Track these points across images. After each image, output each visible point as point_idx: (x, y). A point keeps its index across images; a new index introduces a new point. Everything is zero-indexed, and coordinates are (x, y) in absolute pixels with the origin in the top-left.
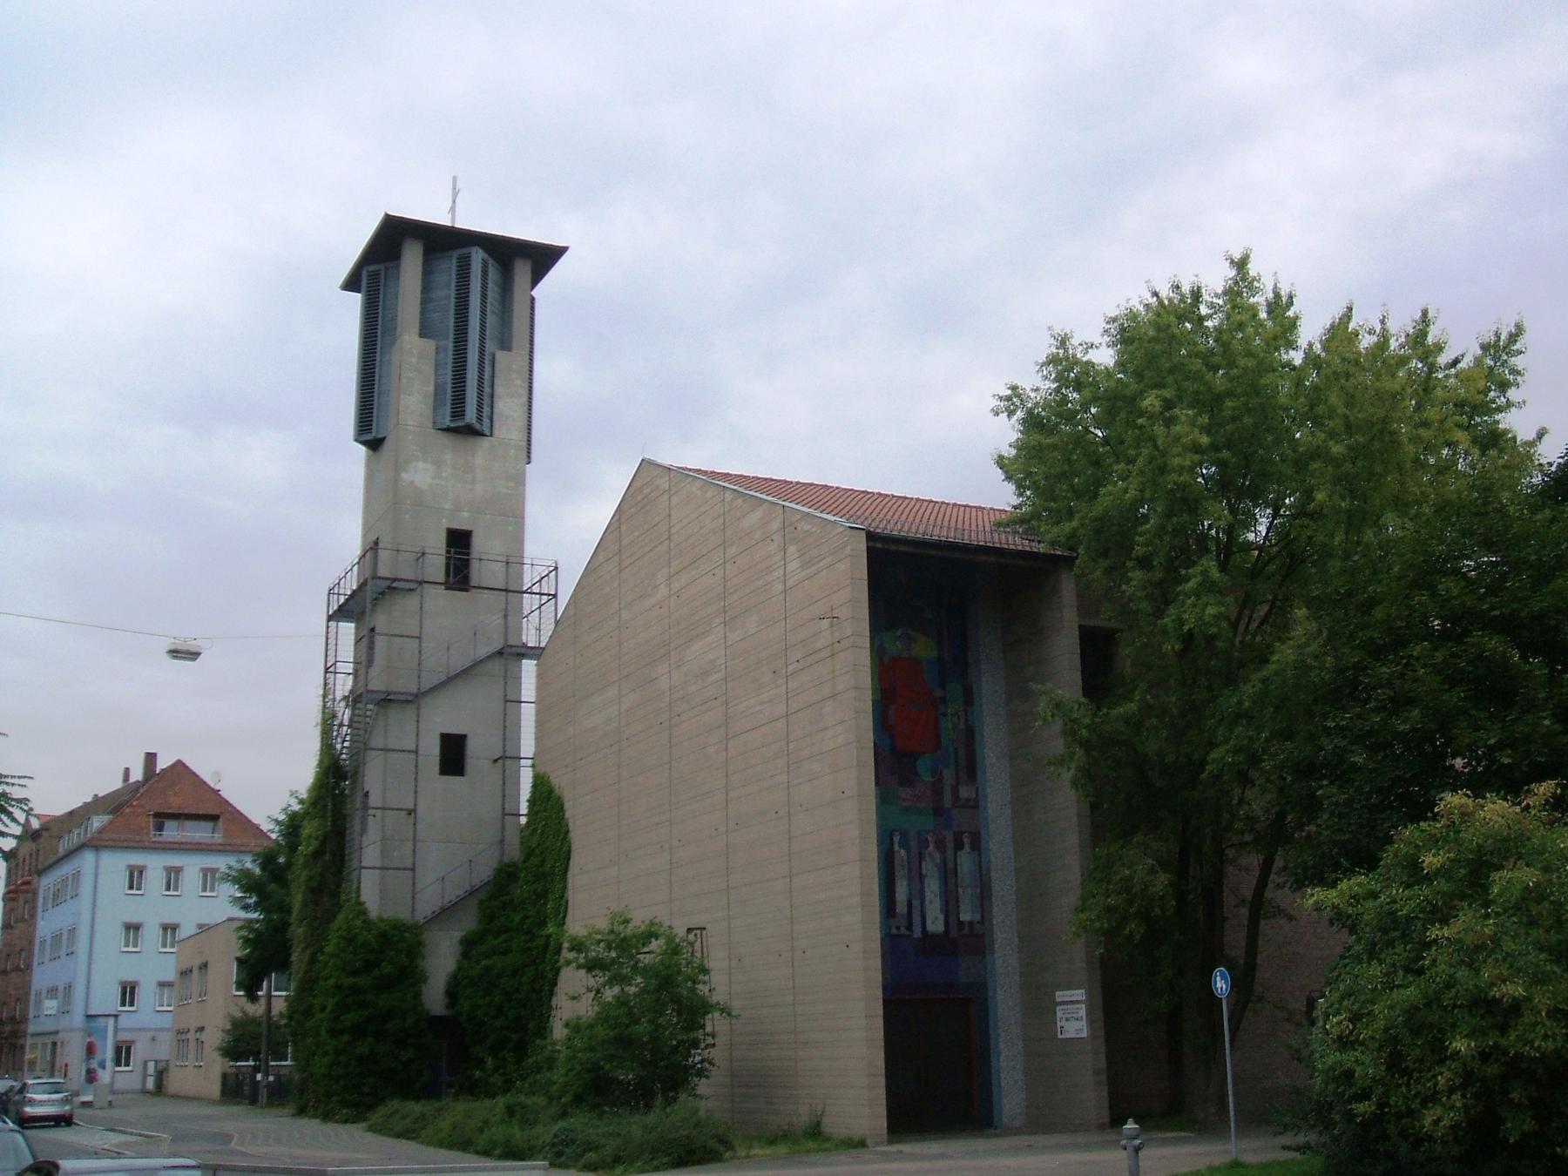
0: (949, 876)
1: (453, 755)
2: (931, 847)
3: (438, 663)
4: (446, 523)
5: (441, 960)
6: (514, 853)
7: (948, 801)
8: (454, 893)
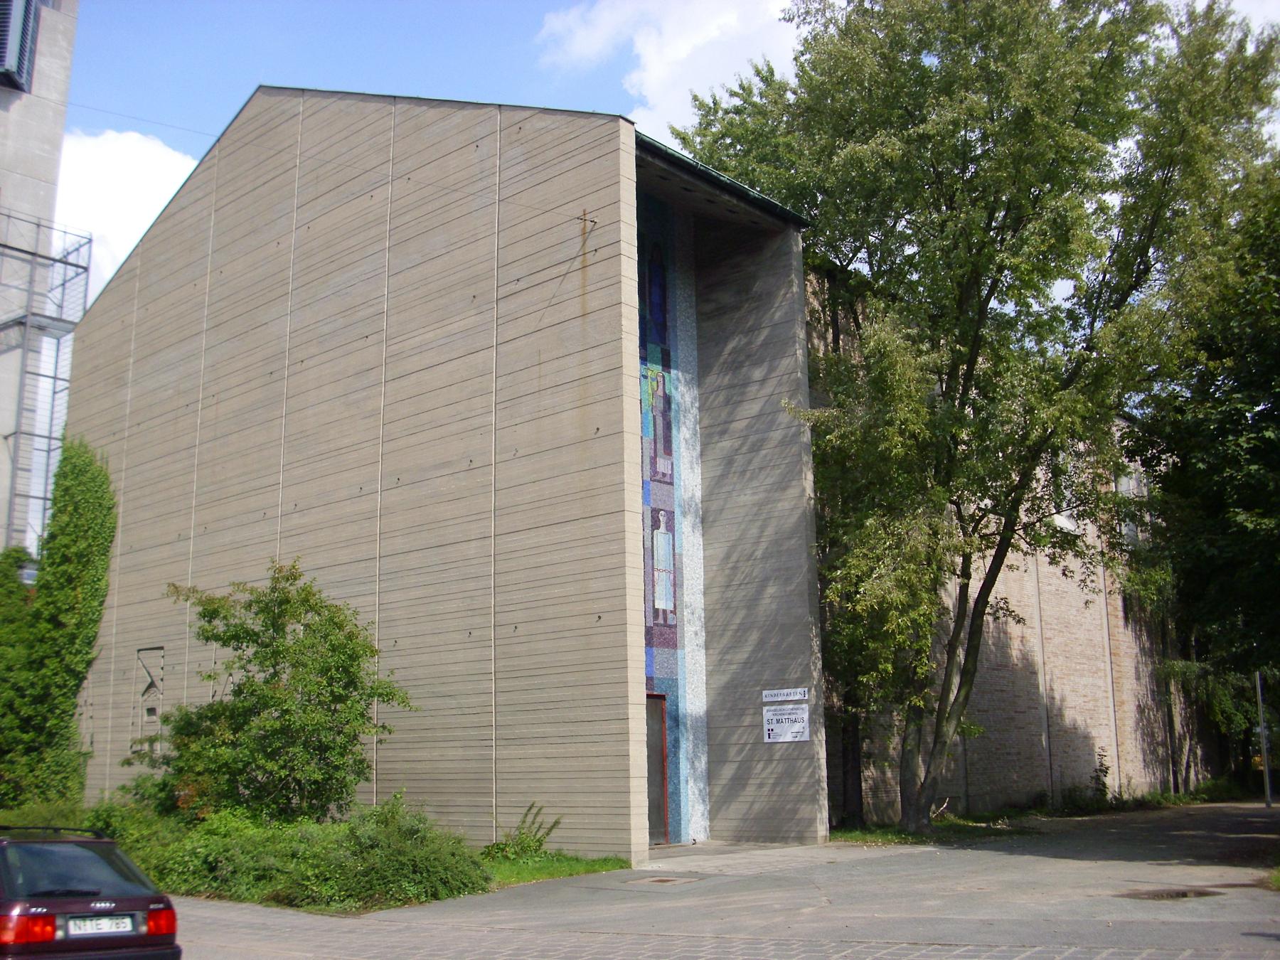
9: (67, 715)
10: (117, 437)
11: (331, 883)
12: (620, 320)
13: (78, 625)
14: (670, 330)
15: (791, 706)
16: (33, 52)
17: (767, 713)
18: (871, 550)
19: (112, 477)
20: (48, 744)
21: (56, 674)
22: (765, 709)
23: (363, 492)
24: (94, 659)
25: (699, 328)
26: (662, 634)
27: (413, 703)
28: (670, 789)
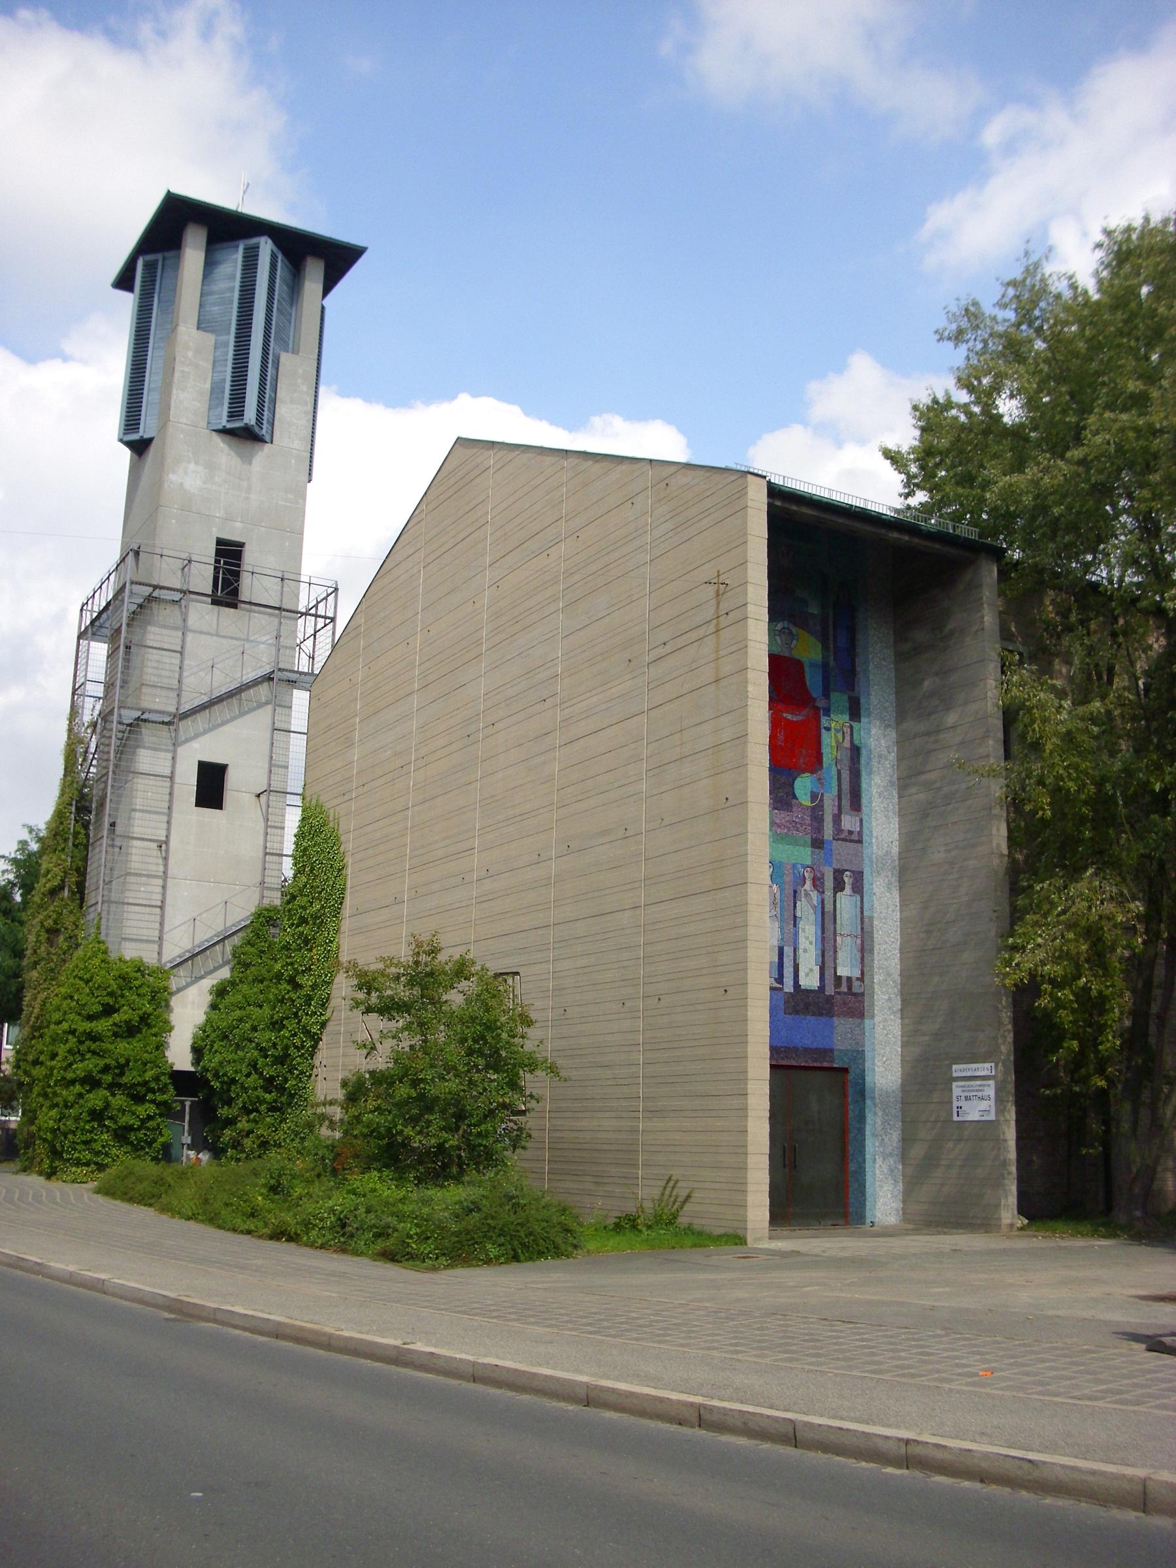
0: (827, 920)
1: (211, 786)
2: (808, 885)
3: (200, 684)
4: (217, 533)
5: (188, 1013)
6: (275, 899)
7: (828, 831)
8: (205, 935)
9: (306, 1075)
10: (346, 797)
11: (430, 1241)
12: (746, 687)
13: (314, 987)
14: (861, 676)
15: (979, 1083)
16: (274, 401)
17: (957, 1089)
18: (1045, 916)
19: (343, 838)
20: (289, 1104)
21: (295, 1035)
22: (954, 1084)
23: (629, 833)
24: (327, 1020)
25: (897, 670)
26: (845, 1003)
27: (563, 1074)
28: (852, 1167)
